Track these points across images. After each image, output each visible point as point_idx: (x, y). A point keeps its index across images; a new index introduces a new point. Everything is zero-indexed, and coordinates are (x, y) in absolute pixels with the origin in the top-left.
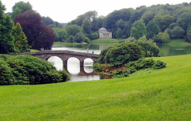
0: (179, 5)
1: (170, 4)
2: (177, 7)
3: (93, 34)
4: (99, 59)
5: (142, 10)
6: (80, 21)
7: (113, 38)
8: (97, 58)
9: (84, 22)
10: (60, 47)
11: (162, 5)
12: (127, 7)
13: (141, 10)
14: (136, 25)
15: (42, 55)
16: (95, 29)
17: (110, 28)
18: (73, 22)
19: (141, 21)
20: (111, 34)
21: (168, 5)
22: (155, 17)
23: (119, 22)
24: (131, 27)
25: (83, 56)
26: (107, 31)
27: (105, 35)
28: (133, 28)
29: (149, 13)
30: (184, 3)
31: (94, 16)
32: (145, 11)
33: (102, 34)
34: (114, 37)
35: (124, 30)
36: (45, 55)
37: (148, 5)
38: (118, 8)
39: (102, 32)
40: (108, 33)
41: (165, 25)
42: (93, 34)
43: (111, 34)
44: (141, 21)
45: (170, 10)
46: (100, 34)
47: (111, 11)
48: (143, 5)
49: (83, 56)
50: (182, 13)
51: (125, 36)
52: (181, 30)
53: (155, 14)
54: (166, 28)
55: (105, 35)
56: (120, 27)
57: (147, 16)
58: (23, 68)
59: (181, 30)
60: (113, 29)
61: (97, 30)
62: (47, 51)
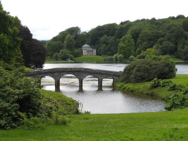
0: (165, 19)
1: (157, 18)
2: (164, 21)
3: (76, 51)
4: (122, 78)
5: (126, 26)
6: (63, 36)
7: (97, 55)
8: (119, 76)
9: (67, 39)
10: (51, 63)
11: (147, 20)
12: (111, 22)
13: (126, 25)
14: (124, 40)
15: (55, 73)
16: (79, 46)
17: (94, 45)
18: (55, 39)
19: (128, 35)
20: (96, 51)
21: (154, 19)
22: (141, 32)
23: (102, 39)
24: (117, 43)
25: (43, 73)
26: (91, 48)
27: (88, 52)
28: (121, 44)
29: (134, 28)
30: (170, 17)
31: (77, 32)
32: (131, 26)
33: (86, 51)
34: (98, 54)
35: (109, 46)
36: (59, 73)
37: (132, 19)
38: (102, 24)
39: (86, 49)
40: (92, 50)
41: (152, 40)
42: (76, 51)
43: (95, 51)
44: (128, 35)
45: (156, 24)
46: (83, 51)
47: (95, 26)
48: (127, 20)
49: (43, 73)
50: (171, 28)
51: (110, 52)
52: (172, 45)
53: (142, 29)
54: (154, 44)
55: (88, 52)
56: (105, 43)
57: (133, 31)
58: (82, 138)
59: (172, 45)
60: (96, 46)
61: (81, 47)
62: (38, 70)
